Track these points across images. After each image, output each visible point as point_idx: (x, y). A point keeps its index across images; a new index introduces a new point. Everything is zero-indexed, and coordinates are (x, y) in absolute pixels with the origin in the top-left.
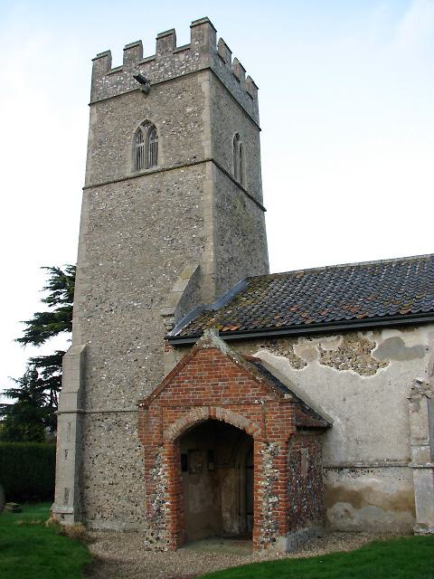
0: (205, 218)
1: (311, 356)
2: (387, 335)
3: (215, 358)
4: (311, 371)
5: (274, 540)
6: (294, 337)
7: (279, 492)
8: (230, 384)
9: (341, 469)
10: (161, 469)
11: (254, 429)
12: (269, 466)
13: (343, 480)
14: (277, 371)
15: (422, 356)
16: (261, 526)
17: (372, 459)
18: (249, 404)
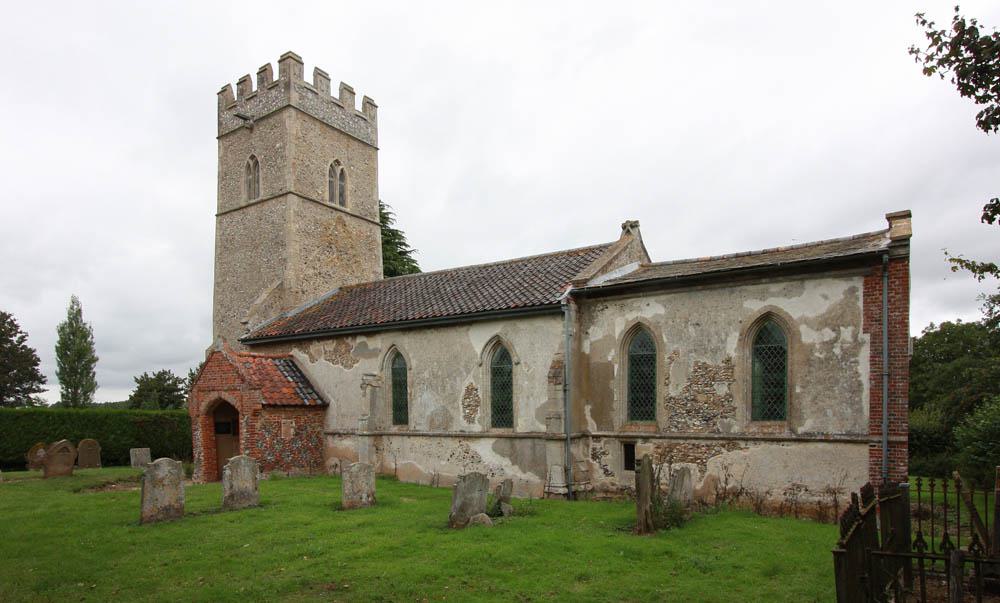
2: (360, 340)
6: (310, 340)
9: (333, 434)
11: (237, 405)
15: (377, 356)
18: (235, 390)
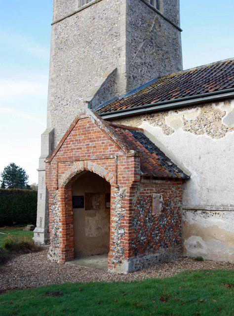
0: (121, 33)
1: (177, 125)
3: (88, 125)
4: (177, 134)
5: (121, 262)
7: (125, 226)
8: (96, 144)
10: (57, 206)
11: (110, 178)
12: (119, 206)
13: (197, 219)
14: (154, 137)
16: (113, 251)
17: (219, 204)
